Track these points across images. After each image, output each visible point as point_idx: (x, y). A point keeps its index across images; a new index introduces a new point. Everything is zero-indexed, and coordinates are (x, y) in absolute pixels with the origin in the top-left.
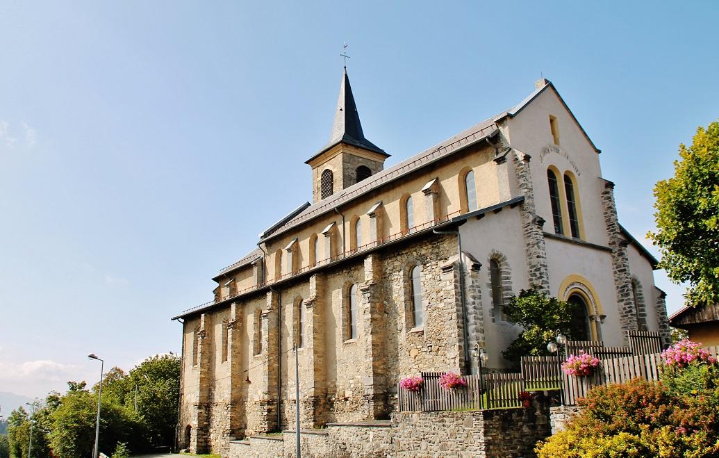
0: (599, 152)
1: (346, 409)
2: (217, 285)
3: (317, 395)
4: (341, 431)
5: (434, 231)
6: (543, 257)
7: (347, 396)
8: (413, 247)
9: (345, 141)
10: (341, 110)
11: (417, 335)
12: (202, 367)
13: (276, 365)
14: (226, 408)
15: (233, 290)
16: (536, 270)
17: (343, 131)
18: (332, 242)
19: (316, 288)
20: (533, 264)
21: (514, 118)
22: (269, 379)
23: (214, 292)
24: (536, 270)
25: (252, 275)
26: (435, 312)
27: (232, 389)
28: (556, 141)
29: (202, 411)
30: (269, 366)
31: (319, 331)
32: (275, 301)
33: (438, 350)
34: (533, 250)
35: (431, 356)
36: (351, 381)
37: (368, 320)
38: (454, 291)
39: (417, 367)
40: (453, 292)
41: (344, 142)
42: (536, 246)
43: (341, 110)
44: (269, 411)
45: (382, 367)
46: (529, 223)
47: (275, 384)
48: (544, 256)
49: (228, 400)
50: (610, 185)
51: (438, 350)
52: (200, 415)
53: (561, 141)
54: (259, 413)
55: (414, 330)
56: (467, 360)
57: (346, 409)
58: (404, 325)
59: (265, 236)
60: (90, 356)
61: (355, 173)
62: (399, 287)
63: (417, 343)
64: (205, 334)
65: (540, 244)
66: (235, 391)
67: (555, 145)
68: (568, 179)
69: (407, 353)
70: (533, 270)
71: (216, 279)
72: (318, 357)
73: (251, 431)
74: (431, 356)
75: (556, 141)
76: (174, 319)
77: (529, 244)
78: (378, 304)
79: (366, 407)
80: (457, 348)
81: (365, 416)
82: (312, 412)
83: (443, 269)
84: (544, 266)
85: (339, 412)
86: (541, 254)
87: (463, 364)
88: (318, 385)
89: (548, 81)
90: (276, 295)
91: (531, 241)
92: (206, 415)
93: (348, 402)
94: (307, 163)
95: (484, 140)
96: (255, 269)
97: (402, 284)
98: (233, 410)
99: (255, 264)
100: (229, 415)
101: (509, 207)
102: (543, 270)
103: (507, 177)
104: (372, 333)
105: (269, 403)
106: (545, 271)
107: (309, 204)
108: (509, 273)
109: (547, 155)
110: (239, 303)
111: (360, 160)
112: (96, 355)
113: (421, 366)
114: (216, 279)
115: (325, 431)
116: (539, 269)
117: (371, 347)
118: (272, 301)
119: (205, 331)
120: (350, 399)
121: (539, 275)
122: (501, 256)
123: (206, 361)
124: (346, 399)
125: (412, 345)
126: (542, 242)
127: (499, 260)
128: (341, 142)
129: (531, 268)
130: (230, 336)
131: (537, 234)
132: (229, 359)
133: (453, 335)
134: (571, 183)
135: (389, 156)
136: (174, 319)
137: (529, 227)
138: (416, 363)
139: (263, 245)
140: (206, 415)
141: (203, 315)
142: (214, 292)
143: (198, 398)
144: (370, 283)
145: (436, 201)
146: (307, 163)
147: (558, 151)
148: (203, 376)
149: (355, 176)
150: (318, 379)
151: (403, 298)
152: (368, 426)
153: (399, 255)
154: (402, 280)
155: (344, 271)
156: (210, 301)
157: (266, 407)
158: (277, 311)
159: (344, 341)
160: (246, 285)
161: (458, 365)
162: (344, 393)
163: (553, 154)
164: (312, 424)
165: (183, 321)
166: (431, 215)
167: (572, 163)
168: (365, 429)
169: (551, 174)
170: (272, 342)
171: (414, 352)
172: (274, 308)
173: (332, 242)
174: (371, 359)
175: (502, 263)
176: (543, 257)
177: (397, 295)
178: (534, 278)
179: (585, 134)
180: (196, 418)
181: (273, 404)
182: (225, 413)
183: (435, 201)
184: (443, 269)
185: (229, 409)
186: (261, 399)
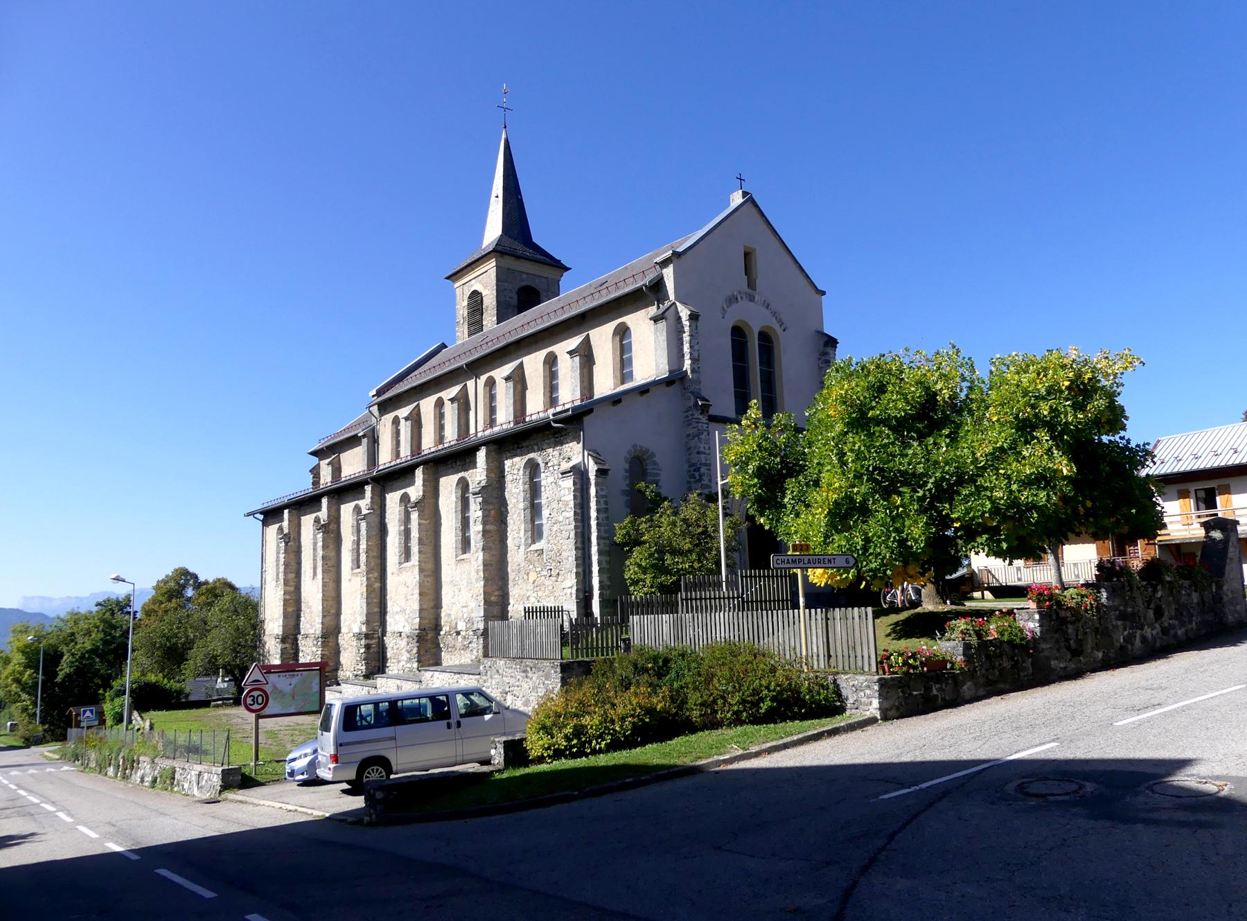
0: (823, 293)
1: (459, 645)
2: (315, 460)
3: (423, 627)
4: (435, 678)
5: (552, 424)
6: (704, 453)
7: (459, 629)
8: (534, 439)
9: (499, 248)
10: (497, 197)
11: (536, 555)
12: (285, 584)
13: (377, 585)
14: (315, 642)
15: (337, 470)
16: (695, 470)
17: (500, 232)
18: (461, 416)
19: (423, 485)
20: (693, 461)
21: (683, 257)
22: (368, 604)
23: (310, 471)
24: (695, 470)
25: (360, 445)
26: (556, 526)
27: (324, 616)
28: (751, 284)
29: (287, 645)
30: (367, 586)
31: (426, 541)
32: (377, 498)
33: (558, 574)
34: (692, 443)
35: (551, 583)
36: (465, 610)
37: (479, 532)
38: (572, 502)
39: (535, 595)
40: (572, 504)
41: (499, 251)
42: (696, 439)
43: (497, 197)
44: (367, 647)
45: (496, 593)
46: (690, 407)
47: (376, 610)
48: (707, 451)
49: (319, 632)
50: (832, 342)
51: (558, 574)
52: (283, 651)
53: (760, 283)
54: (355, 650)
55: (534, 547)
56: (587, 589)
57: (459, 645)
58: (523, 540)
59: (379, 393)
60: (114, 579)
61: (515, 297)
62: (517, 491)
63: (536, 565)
64: (289, 538)
65: (702, 437)
66: (328, 619)
67: (750, 291)
68: (766, 339)
69: (525, 577)
70: (692, 469)
71: (314, 453)
72: (425, 576)
73: (348, 674)
74: (551, 583)
75: (751, 284)
76: (249, 515)
77: (689, 435)
78: (493, 512)
79: (474, 645)
80: (574, 576)
81: (474, 657)
82: (415, 650)
83: (562, 474)
84: (705, 465)
85: (450, 649)
86: (702, 450)
87: (581, 596)
88: (425, 614)
89: (748, 193)
90: (378, 488)
91: (691, 431)
92: (292, 652)
93: (460, 637)
94: (447, 278)
95: (639, 290)
96: (365, 441)
97: (521, 488)
98: (324, 645)
99: (364, 436)
100: (319, 652)
101: (664, 385)
102: (703, 470)
103: (665, 343)
104: (483, 549)
105: (367, 636)
106: (706, 471)
107: (444, 346)
108: (657, 475)
109: (735, 306)
110: (333, 497)
111: (524, 276)
112: (122, 577)
113: (540, 593)
114: (314, 453)
115: (15, 733)
116: (698, 470)
117: (481, 567)
118: (372, 498)
119: (289, 533)
120: (463, 633)
121: (698, 477)
122: (647, 451)
123: (292, 576)
124: (458, 633)
125: (531, 567)
126: (705, 433)
127: (645, 457)
128: (494, 251)
129: (689, 466)
130: (320, 544)
131: (697, 422)
132: (320, 576)
133: (570, 558)
134: (772, 342)
135: (567, 269)
136: (249, 515)
137: (690, 412)
138: (535, 589)
139: (375, 409)
140: (292, 652)
141: (286, 511)
142: (310, 471)
143: (281, 628)
144: (483, 484)
145: (584, 367)
146: (447, 278)
147: (752, 299)
148: (288, 597)
149: (514, 301)
150: (425, 607)
151: (521, 506)
152: (459, 673)
153: (518, 448)
154: (521, 481)
155: (458, 463)
156: (302, 486)
157: (363, 642)
158: (379, 512)
159: (457, 556)
160: (353, 464)
161: (574, 596)
162: (456, 623)
163: (744, 304)
164: (415, 665)
165: (261, 517)
166: (576, 386)
167: (774, 314)
168: (457, 676)
169: (738, 334)
170: (371, 554)
171: (533, 576)
172: (375, 507)
173: (462, 413)
174: (482, 583)
175: (648, 462)
176: (704, 453)
177: (515, 501)
178: (693, 480)
179: (800, 267)
180: (278, 656)
181: (373, 638)
182: (314, 649)
183: (582, 366)
184: (562, 474)
185: (320, 643)
186: (358, 631)
